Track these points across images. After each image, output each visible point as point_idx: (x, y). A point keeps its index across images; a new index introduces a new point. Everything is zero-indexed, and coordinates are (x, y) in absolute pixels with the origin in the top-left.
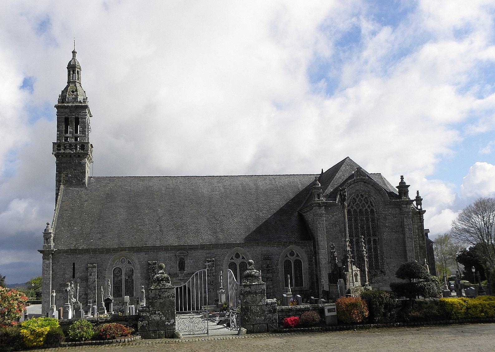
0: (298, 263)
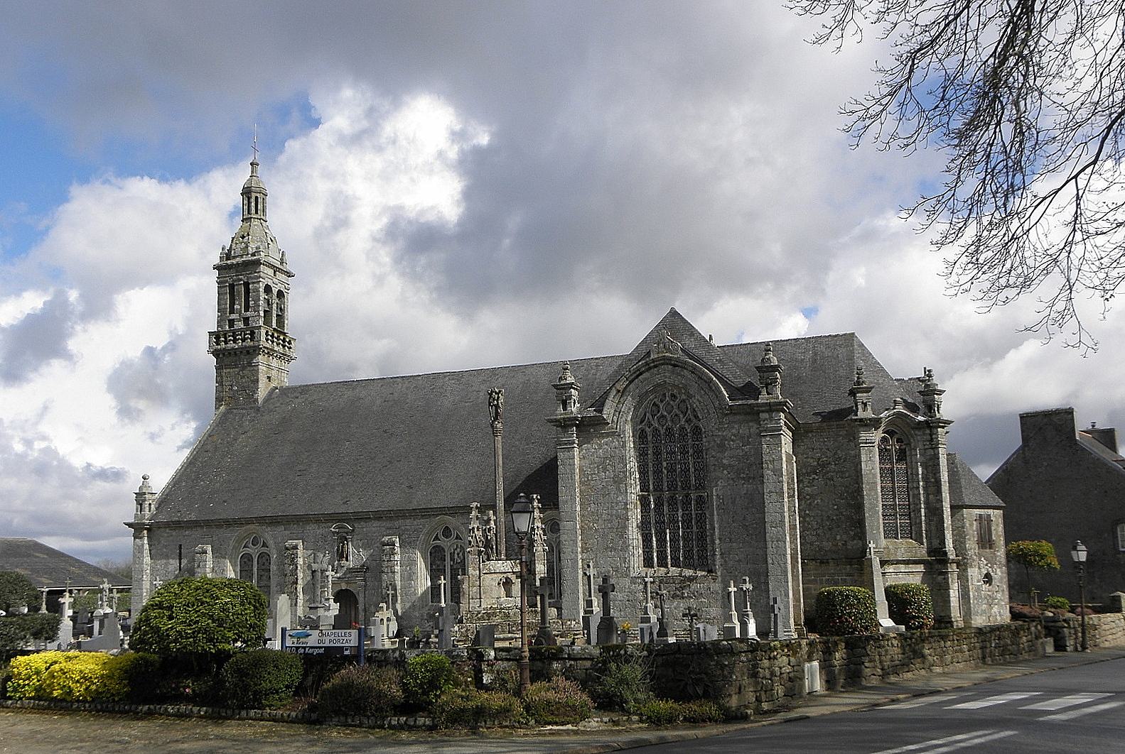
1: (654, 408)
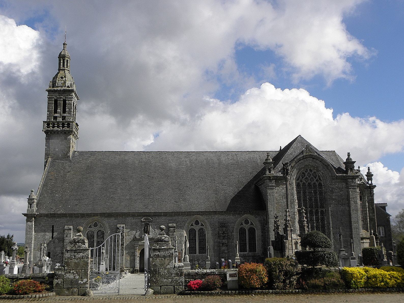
0: (252, 231)
1: (303, 175)
